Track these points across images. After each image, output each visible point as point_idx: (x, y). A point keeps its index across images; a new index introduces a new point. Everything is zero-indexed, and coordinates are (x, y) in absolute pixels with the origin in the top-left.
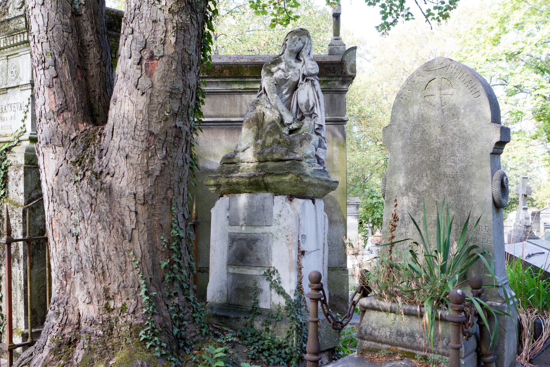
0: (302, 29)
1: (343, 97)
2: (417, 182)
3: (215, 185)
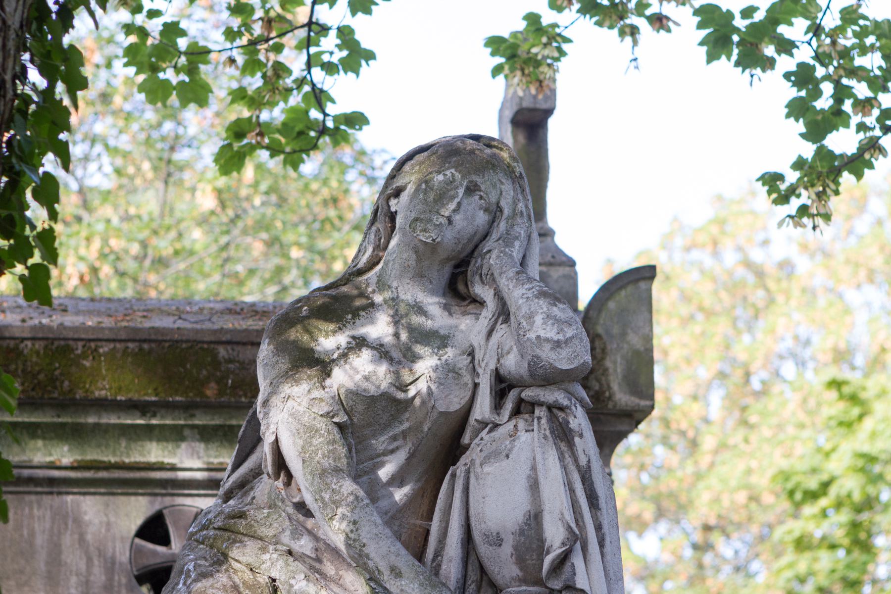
0: (476, 138)
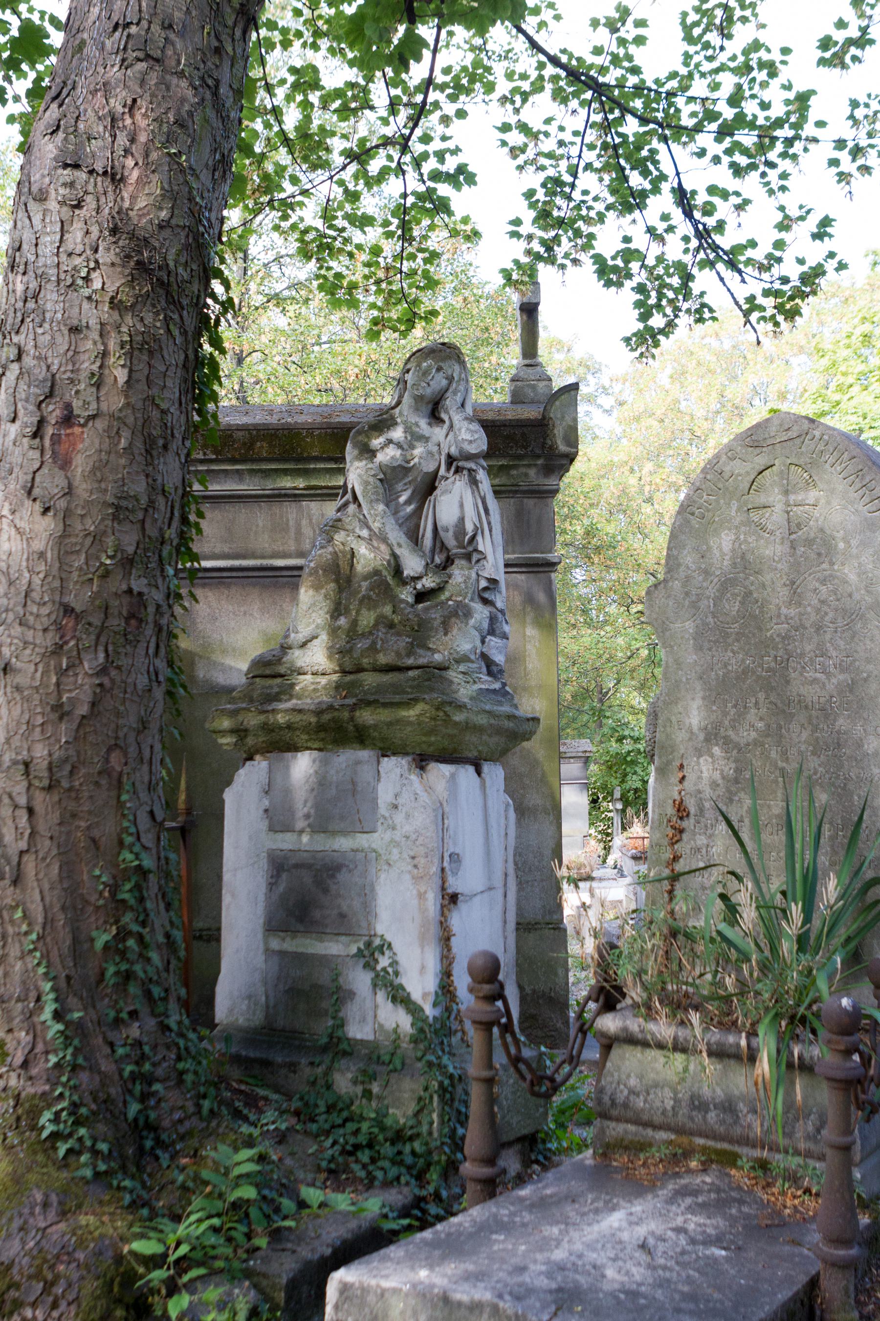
0: (443, 344)
2: (734, 720)
3: (232, 731)
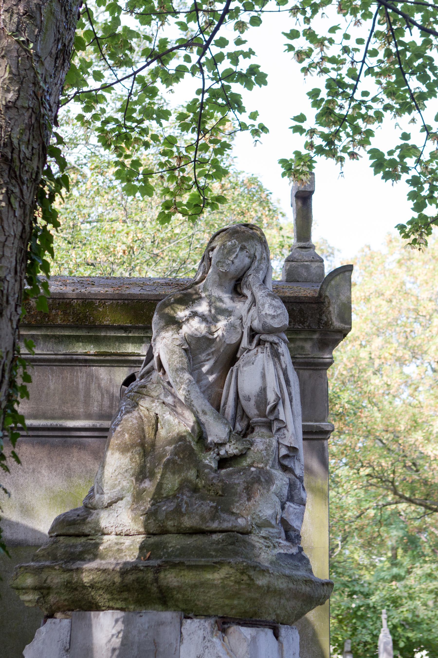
0: (246, 225)
1: (321, 377)
3: (35, 589)
